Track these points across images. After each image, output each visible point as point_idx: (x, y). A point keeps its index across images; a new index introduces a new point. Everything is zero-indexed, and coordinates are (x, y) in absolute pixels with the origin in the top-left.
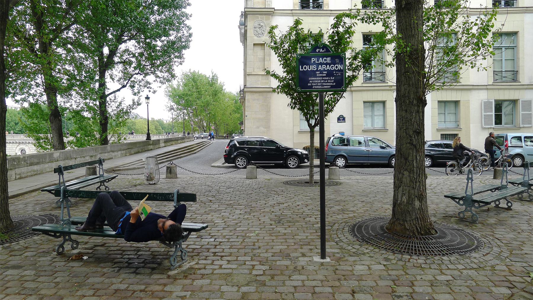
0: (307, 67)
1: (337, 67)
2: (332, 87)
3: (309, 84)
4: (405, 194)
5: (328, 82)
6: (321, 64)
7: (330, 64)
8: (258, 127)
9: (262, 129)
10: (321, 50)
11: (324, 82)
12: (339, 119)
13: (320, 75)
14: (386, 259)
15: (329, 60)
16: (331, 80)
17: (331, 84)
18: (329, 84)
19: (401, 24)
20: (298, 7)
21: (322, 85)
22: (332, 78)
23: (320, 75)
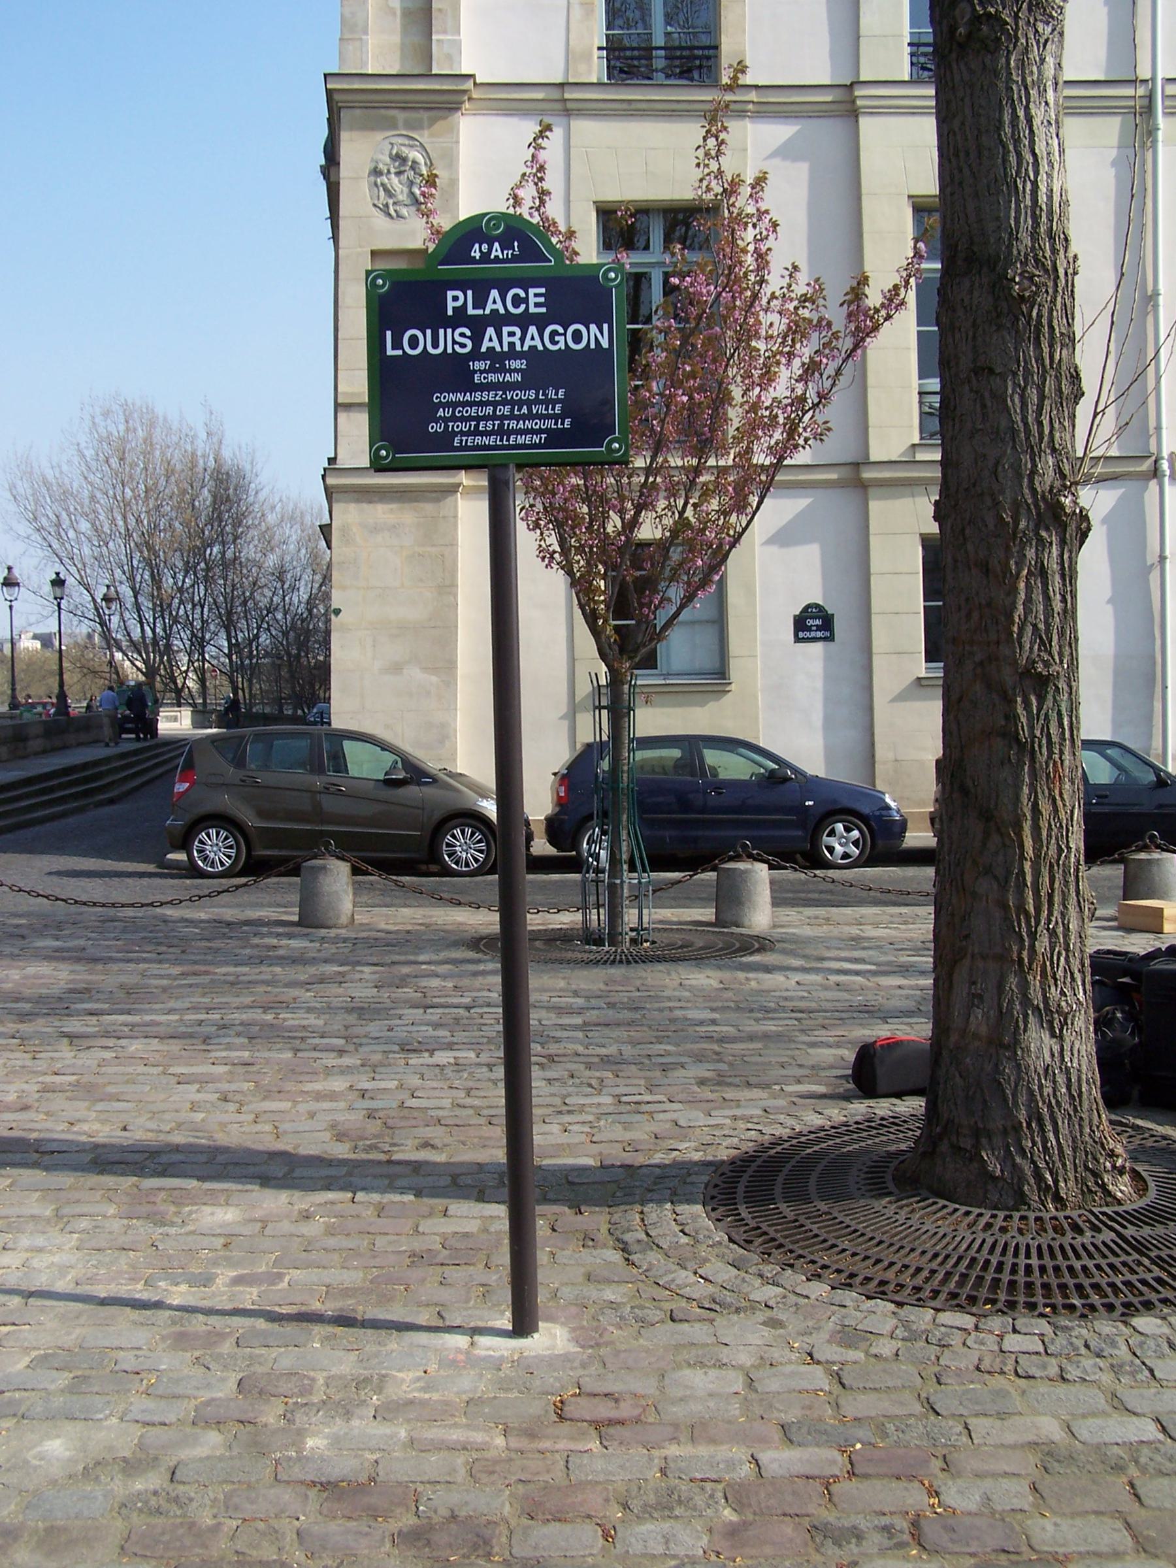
0: (425, 340)
1: (577, 337)
2: (555, 438)
3: (434, 428)
4: (980, 997)
5: (530, 416)
6: (499, 321)
7: (541, 322)
8: (396, 668)
9: (415, 674)
10: (497, 251)
11: (512, 417)
12: (800, 624)
13: (492, 378)
14: (849, 1336)
15: (535, 297)
16: (547, 402)
17: (550, 424)
18: (537, 424)
19: (956, 124)
20: (595, 69)
21: (501, 432)
22: (551, 393)
23: (492, 378)
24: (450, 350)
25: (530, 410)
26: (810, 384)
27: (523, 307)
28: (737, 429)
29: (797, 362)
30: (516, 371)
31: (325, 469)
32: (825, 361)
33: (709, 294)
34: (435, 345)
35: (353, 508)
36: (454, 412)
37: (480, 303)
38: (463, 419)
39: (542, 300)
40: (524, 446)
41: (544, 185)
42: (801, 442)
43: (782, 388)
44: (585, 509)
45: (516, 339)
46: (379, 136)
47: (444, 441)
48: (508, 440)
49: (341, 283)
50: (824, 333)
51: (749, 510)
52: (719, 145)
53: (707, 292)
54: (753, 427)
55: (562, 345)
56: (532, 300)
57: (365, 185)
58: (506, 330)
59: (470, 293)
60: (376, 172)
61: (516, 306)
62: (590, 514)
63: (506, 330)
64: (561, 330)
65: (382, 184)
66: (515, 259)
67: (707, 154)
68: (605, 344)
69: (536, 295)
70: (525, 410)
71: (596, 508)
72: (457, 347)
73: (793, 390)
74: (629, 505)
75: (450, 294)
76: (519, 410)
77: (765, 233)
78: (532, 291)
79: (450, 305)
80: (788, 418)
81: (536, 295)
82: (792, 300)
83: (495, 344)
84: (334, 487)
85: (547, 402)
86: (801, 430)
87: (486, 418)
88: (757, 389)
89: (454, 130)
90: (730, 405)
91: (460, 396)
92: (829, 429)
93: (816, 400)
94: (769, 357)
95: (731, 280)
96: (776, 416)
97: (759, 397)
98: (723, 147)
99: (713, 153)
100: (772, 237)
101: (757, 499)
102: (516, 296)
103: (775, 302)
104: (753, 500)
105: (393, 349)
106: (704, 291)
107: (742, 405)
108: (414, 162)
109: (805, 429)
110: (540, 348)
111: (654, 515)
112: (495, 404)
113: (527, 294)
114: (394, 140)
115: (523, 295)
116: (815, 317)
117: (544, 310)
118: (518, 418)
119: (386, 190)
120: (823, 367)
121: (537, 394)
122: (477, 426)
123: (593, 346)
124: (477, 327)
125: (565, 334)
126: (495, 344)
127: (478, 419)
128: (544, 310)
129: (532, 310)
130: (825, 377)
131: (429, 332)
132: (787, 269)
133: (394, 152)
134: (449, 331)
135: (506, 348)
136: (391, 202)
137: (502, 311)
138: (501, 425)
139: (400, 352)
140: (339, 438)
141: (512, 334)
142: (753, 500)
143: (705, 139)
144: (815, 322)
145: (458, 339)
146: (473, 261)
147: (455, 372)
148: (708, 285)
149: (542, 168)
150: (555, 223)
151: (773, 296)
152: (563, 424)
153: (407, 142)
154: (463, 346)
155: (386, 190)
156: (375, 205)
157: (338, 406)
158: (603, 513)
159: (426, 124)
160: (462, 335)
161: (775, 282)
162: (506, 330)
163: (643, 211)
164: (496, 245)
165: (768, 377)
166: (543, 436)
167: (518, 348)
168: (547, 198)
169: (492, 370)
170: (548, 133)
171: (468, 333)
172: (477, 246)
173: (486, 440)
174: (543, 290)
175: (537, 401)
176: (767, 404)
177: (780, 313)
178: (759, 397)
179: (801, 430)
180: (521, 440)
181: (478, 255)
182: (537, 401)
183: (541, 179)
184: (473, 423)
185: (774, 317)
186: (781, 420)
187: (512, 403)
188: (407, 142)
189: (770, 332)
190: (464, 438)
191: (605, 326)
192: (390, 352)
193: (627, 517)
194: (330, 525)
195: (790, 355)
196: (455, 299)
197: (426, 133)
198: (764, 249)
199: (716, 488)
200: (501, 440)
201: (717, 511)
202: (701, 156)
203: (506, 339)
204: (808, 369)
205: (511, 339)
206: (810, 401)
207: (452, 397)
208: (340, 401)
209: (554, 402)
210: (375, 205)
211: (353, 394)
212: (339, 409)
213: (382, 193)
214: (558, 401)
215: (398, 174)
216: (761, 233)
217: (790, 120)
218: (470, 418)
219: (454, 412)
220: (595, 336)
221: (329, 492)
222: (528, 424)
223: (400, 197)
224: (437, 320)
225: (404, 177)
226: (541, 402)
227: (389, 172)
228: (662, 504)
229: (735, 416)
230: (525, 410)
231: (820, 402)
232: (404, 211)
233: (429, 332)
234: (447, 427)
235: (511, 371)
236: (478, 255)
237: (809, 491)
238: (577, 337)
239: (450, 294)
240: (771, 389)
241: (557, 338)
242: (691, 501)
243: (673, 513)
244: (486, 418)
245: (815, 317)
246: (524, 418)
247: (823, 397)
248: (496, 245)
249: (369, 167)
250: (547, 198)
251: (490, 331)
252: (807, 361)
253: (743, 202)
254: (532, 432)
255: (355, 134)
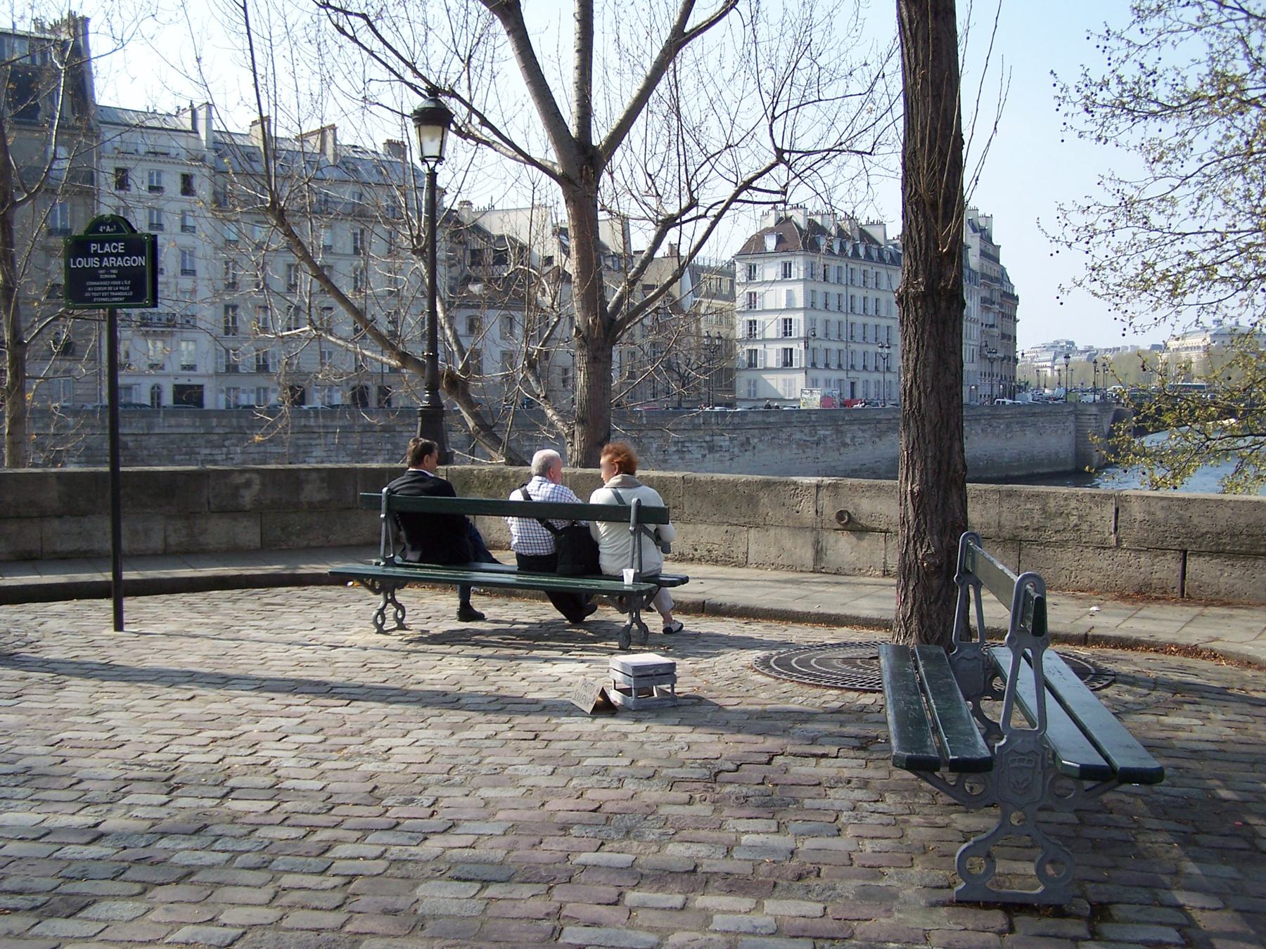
0: (83, 261)
3: (87, 294)
6: (108, 255)
7: (122, 255)
15: (121, 246)
21: (110, 296)
47: (90, 299)
147: (93, 274)
224: (88, 254)
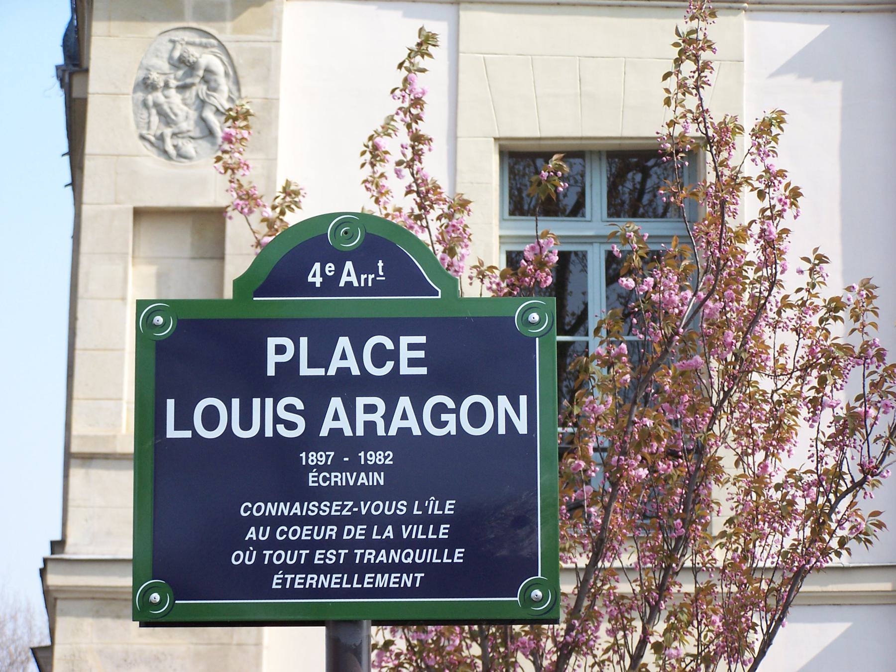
0: (229, 415)
1: (477, 415)
2: (438, 580)
3: (241, 558)
5: (398, 543)
6: (349, 386)
7: (418, 390)
10: (349, 275)
11: (368, 543)
13: (337, 478)
15: (409, 349)
16: (427, 520)
17: (431, 556)
18: (410, 556)
21: (350, 567)
23: (337, 478)
24: (269, 433)
25: (398, 532)
26: (849, 452)
27: (390, 365)
28: (730, 521)
29: (826, 416)
30: (376, 468)
31: (45, 561)
32: (872, 412)
33: (683, 301)
34: (246, 424)
35: (88, 624)
36: (273, 533)
37: (320, 358)
38: (288, 545)
39: (421, 354)
40: (386, 592)
41: (422, 128)
42: (834, 544)
43: (800, 454)
44: (476, 650)
45: (377, 418)
46: (154, 29)
47: (256, 580)
48: (361, 581)
49: (83, 260)
50: (872, 368)
51: (747, 655)
52: (700, 70)
53: (681, 299)
54: (751, 521)
55: (451, 428)
56: (405, 355)
57: (127, 105)
58: (361, 402)
59: (304, 341)
60: (147, 85)
61: (379, 364)
62: (483, 657)
63: (361, 402)
64: (451, 404)
65: (157, 105)
66: (377, 289)
67: (682, 86)
68: (522, 427)
69: (411, 347)
70: (389, 532)
71: (495, 648)
72: (281, 429)
73: (820, 459)
74: (549, 645)
75: (272, 342)
76: (381, 532)
77: (779, 207)
78: (405, 341)
79: (272, 359)
80: (813, 505)
81: (411, 347)
82: (816, 309)
83: (343, 423)
84: (61, 589)
85: (427, 520)
86: (834, 526)
87: (326, 544)
88: (760, 456)
89: (272, 22)
90: (717, 480)
91: (284, 508)
92: (880, 525)
93: (859, 477)
94: (779, 403)
95: (722, 272)
96: (792, 503)
97: (764, 467)
98: (707, 72)
99: (691, 83)
100: (790, 213)
101: (760, 636)
102: (379, 347)
103: (789, 313)
104: (756, 638)
105: (177, 428)
106: (676, 299)
107: (737, 479)
108: (208, 71)
109: (840, 524)
110: (417, 432)
111: (590, 660)
112: (340, 522)
113: (397, 344)
114: (178, 36)
115: (390, 345)
116: (857, 342)
117: (423, 371)
118: (378, 546)
119: (162, 114)
120: (869, 422)
121: (410, 508)
122: (310, 557)
123: (502, 430)
124: (316, 395)
125: (456, 411)
126: (343, 423)
127: (313, 545)
128: (423, 371)
129: (405, 370)
130: (872, 438)
131: (236, 402)
132: (807, 260)
133: (177, 54)
134: (269, 402)
135: (360, 432)
136: (168, 132)
137: (356, 371)
138: (350, 557)
139: (187, 434)
140: (71, 510)
141: (370, 409)
142: (756, 638)
143: (678, 62)
144: (857, 350)
145: (283, 414)
146: (311, 289)
147: (276, 466)
148: (682, 289)
149: (417, 102)
150: (436, 188)
151: (785, 304)
152: (451, 556)
153: (197, 40)
154: (291, 426)
155: (162, 114)
156: (142, 137)
157: (69, 457)
158: (505, 657)
159: (229, 9)
160: (290, 408)
161: (792, 281)
162: (361, 402)
163: (577, 153)
164: (349, 265)
165: (779, 436)
166: (419, 576)
167: (381, 432)
168: (425, 148)
169: (337, 466)
170: (431, 49)
171: (300, 405)
172: (317, 266)
173: (324, 581)
174: (422, 339)
175: (409, 519)
176: (778, 479)
177: (797, 331)
178: (764, 467)
179: (834, 526)
180: (381, 581)
181: (318, 281)
182: (409, 519)
183: (417, 118)
184: (304, 552)
185: (788, 338)
186: (801, 505)
187: (369, 520)
188: (197, 40)
189: (782, 360)
190: (289, 577)
191: (523, 399)
192: (172, 433)
193: (545, 663)
194: (50, 649)
195: (816, 404)
196: (280, 350)
197: (229, 25)
198: (775, 232)
199: (695, 608)
200: (350, 581)
201: (695, 657)
202: (673, 88)
203: (361, 418)
204: (845, 426)
205: (370, 417)
206: (848, 478)
207: (271, 509)
208: (74, 448)
209: (437, 521)
210: (142, 137)
211: (96, 438)
212: (73, 461)
213: (155, 119)
214: (444, 519)
215: (183, 88)
216: (772, 208)
217: (809, 15)
218: (299, 544)
219: (273, 533)
220: (505, 414)
221: (51, 598)
222: (395, 556)
223: (184, 126)
225: (191, 94)
226: (416, 520)
227: (167, 86)
228: (603, 639)
229: (724, 499)
230: (389, 532)
231: (864, 480)
232: (189, 147)
233: (236, 402)
234: (260, 557)
235: (369, 469)
236: (318, 281)
237: (846, 610)
238: (477, 415)
239: (272, 342)
240: (783, 455)
241: (444, 417)
242: (652, 640)
243: (622, 657)
244: (326, 544)
245: (857, 342)
246: (388, 545)
247: (870, 471)
248: (349, 265)
249: (137, 75)
250: (425, 148)
251: (336, 403)
252: (842, 413)
253: (742, 157)
254: (400, 568)
255: (115, 26)
